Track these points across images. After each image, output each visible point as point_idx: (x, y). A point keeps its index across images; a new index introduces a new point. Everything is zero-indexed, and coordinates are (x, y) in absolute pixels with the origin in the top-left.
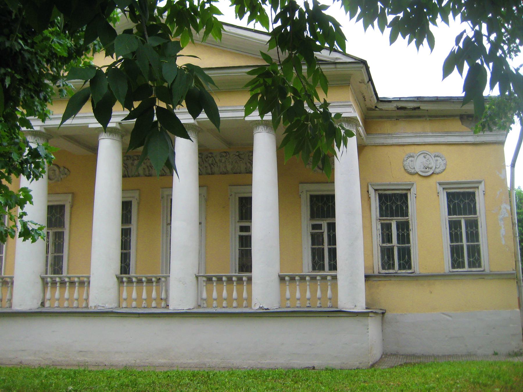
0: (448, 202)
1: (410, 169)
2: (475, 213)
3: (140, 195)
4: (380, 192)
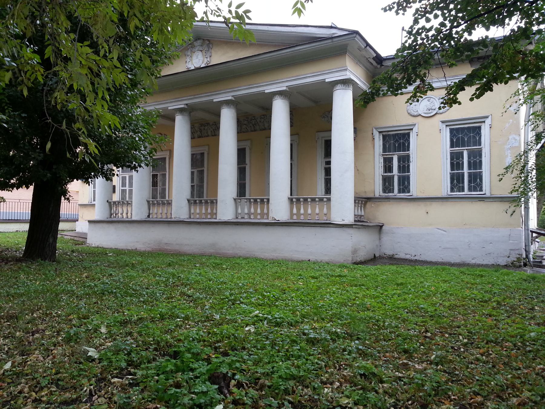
0: (450, 136)
1: (413, 112)
2: (480, 144)
3: (209, 149)
4: (384, 133)
